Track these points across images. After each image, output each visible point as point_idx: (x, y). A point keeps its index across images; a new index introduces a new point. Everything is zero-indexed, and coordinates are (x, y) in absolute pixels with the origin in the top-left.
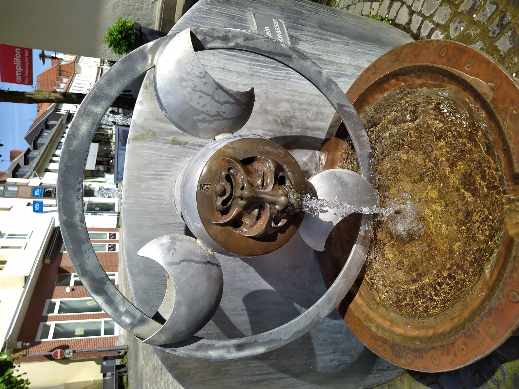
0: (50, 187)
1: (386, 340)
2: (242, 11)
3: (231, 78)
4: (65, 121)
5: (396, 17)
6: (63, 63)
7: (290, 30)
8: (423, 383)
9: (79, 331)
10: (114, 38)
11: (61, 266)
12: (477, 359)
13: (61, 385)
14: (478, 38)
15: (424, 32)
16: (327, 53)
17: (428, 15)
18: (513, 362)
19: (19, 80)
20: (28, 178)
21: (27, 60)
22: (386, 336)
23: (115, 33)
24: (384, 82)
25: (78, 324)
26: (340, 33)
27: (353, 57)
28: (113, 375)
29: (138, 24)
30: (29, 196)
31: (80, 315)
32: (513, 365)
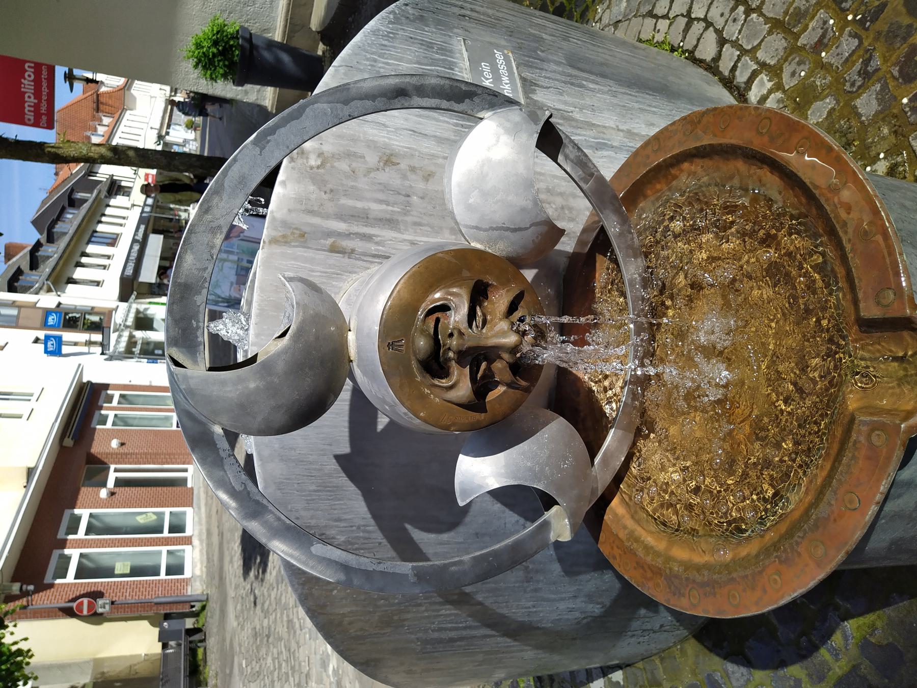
0: (75, 310)
1: (660, 569)
2: (445, 35)
3: (426, 147)
4: (104, 193)
5: (696, 46)
6: (103, 89)
7: (521, 68)
8: (718, 655)
9: (121, 567)
10: (204, 53)
11: (93, 451)
12: (796, 594)
13: (88, 662)
14: (828, 91)
15: (741, 76)
16: (581, 109)
17: (749, 47)
18: (861, 618)
19: (29, 120)
20: (37, 293)
21: (45, 84)
22: (659, 562)
23: (205, 44)
24: (672, 165)
25: (120, 555)
26: (603, 76)
27: (624, 116)
28: (179, 645)
29: (246, 29)
30: (38, 325)
31: (125, 539)
32: (861, 622)
